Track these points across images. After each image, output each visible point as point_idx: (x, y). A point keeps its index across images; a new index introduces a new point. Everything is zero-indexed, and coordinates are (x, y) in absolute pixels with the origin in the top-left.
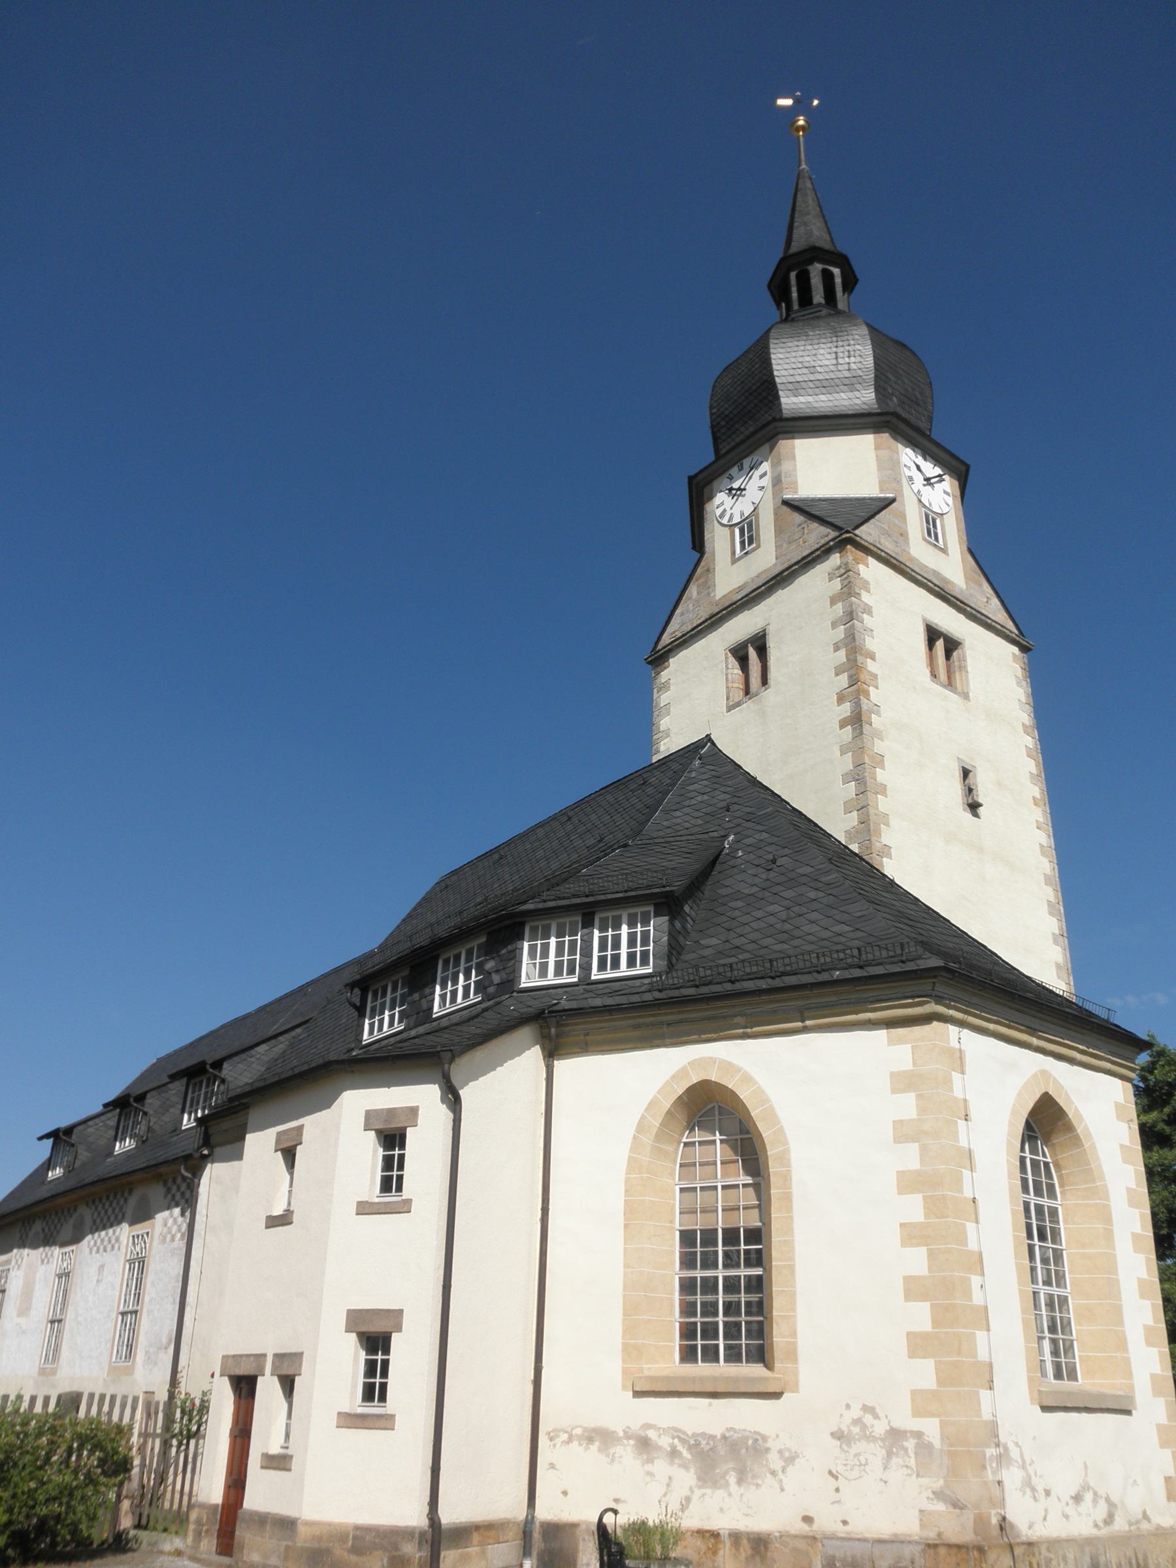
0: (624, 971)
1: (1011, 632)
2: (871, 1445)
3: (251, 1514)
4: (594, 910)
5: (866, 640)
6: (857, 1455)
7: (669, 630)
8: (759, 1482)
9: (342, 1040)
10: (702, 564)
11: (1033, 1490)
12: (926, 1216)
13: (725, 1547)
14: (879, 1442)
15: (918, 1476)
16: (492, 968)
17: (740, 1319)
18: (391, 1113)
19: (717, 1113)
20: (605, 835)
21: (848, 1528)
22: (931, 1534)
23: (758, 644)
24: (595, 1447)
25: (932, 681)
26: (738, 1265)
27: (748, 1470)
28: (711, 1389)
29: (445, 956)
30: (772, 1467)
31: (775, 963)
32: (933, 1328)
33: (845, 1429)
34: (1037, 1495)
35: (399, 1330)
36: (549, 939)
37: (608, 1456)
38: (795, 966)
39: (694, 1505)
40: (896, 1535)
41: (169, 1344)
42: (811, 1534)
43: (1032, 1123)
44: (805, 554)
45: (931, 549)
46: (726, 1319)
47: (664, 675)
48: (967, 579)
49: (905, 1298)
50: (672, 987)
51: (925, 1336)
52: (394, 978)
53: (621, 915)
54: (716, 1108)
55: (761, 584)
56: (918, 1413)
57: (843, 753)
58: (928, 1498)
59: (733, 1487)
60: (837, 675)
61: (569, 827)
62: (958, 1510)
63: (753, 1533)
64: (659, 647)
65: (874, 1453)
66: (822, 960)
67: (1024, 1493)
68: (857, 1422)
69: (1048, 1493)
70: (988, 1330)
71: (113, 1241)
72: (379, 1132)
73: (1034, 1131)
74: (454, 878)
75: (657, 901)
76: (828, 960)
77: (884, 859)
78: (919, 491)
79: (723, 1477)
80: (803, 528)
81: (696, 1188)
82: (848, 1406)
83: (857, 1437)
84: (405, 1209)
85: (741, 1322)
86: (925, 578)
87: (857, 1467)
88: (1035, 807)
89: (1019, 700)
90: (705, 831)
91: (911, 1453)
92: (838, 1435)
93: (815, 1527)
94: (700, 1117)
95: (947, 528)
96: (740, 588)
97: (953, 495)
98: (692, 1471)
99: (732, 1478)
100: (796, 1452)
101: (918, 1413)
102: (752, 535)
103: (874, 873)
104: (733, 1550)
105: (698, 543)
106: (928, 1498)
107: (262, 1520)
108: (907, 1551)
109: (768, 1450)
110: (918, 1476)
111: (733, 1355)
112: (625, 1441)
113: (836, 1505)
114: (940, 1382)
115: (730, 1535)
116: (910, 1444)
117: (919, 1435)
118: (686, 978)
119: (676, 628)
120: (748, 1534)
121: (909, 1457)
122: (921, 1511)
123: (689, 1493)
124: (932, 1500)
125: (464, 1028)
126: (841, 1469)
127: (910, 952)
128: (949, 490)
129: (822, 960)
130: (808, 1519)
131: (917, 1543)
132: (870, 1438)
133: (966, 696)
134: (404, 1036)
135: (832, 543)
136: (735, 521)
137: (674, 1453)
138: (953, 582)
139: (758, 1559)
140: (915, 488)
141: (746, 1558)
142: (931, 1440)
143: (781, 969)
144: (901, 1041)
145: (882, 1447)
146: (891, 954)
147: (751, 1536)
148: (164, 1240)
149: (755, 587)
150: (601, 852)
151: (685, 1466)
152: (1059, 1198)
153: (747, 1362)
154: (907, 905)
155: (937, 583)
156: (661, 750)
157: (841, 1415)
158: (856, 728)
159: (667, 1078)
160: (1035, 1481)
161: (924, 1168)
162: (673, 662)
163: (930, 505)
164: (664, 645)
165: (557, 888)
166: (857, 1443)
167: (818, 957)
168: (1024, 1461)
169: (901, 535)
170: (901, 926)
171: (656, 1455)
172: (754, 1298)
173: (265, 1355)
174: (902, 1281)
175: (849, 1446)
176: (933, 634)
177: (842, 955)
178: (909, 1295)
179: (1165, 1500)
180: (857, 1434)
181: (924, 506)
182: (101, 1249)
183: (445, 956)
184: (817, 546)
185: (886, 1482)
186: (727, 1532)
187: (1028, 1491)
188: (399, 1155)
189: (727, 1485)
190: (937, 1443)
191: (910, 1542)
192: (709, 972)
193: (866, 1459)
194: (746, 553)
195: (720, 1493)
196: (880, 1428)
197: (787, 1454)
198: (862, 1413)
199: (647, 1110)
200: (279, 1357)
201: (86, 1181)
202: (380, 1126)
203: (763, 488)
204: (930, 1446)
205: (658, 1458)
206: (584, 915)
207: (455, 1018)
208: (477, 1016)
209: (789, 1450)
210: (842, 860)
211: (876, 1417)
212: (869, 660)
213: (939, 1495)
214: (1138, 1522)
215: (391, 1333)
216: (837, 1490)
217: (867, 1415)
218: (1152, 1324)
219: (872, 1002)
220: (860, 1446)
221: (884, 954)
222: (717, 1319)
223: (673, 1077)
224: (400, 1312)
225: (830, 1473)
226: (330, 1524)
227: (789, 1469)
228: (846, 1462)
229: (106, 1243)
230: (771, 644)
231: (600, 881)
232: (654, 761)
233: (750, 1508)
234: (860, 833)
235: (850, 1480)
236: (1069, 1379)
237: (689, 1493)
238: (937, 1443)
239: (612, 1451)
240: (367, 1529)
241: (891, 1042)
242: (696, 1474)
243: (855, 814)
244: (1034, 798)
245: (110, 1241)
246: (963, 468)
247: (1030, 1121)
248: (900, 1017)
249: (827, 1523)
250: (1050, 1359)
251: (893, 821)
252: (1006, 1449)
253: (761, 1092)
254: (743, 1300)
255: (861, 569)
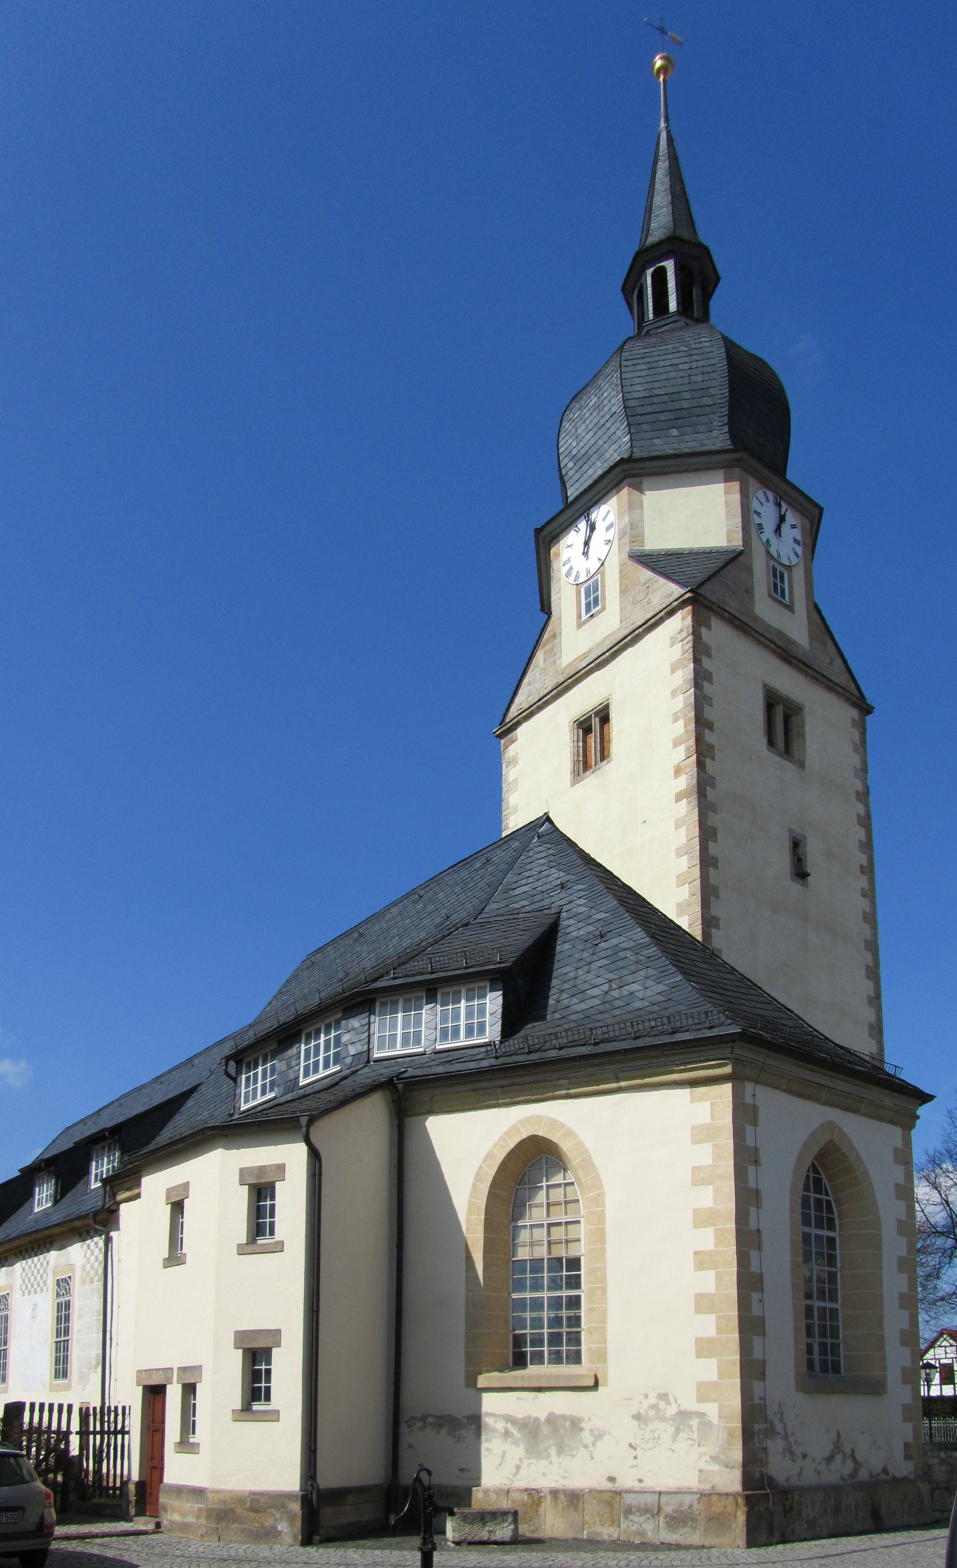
0: (463, 1041)
1: (853, 695)
2: (664, 1424)
3: (170, 1487)
4: (436, 986)
5: (705, 709)
6: (652, 1431)
7: (517, 700)
8: (574, 1453)
9: (224, 1107)
10: (549, 628)
11: (792, 1454)
12: (716, 1245)
13: (546, 1500)
14: (670, 1421)
15: (699, 1445)
16: (348, 1040)
17: (543, 1331)
18: (262, 1169)
19: (544, 1162)
20: (451, 913)
21: (642, 1485)
22: (706, 1487)
23: (602, 715)
24: (444, 1431)
25: (768, 749)
26: (561, 1288)
27: (566, 1444)
28: (536, 1385)
29: (308, 1031)
30: (585, 1441)
31: (594, 1031)
32: (717, 1334)
33: (642, 1411)
34: (795, 1457)
35: (279, 1345)
36: (422, 1010)
37: (454, 1437)
38: (612, 1034)
39: (523, 1471)
40: (679, 1488)
41: (98, 1365)
42: (613, 1489)
43: (817, 1165)
44: (649, 616)
45: (777, 606)
46: (550, 1331)
47: (512, 751)
48: (812, 637)
49: (695, 1311)
50: (505, 1054)
51: (711, 1341)
52: (264, 1052)
53: (398, 1000)
54: (544, 1158)
55: (605, 650)
56: (701, 1399)
57: (677, 827)
58: (706, 1461)
59: (554, 1458)
60: (675, 746)
61: (420, 906)
62: (729, 1470)
63: (569, 1490)
64: (508, 720)
65: (665, 1430)
66: (636, 1028)
67: (784, 1457)
68: (654, 1407)
69: (804, 1456)
70: (764, 1335)
71: (42, 1285)
72: (252, 1186)
73: (819, 1173)
74: (319, 956)
75: (492, 977)
76: (641, 1027)
77: (713, 930)
78: (768, 541)
79: (546, 1450)
80: (648, 587)
81: (527, 1225)
82: (646, 1396)
83: (652, 1418)
84: (278, 1249)
85: (563, 1332)
86: (768, 639)
87: (651, 1441)
88: (860, 874)
89: (855, 767)
90: (540, 909)
91: (695, 1429)
92: (637, 1417)
93: (617, 1485)
94: (530, 1167)
95: (795, 585)
96: (585, 655)
97: (804, 544)
98: (522, 1446)
99: (553, 1451)
100: (603, 1430)
101: (701, 1399)
102: (598, 596)
103: (696, 945)
104: (553, 1503)
105: (546, 607)
106: (706, 1461)
107: (179, 1490)
108: (687, 1499)
109: (581, 1429)
110: (699, 1445)
111: (557, 1358)
112: (469, 1426)
113: (634, 1468)
114: (721, 1376)
115: (550, 1492)
116: (694, 1422)
117: (701, 1415)
118: (517, 1046)
119: (522, 700)
120: (564, 1491)
121: (693, 1432)
122: (701, 1471)
123: (519, 1463)
124: (709, 1463)
125: (322, 1095)
126: (639, 1442)
127: (713, 1020)
128: (799, 538)
129: (636, 1028)
130: (612, 1479)
131: (696, 1493)
132: (662, 1419)
133: (801, 765)
134: (275, 1102)
135: (676, 603)
136: (581, 580)
137: (507, 1434)
138: (797, 643)
139: (572, 1508)
140: (764, 537)
141: (563, 1508)
142: (711, 1419)
143: (600, 1037)
144: (702, 1099)
145: (672, 1425)
146: (696, 1021)
147: (567, 1492)
148: (84, 1283)
149: (600, 653)
150: (447, 930)
151: (516, 1443)
152: (837, 1230)
153: (567, 1363)
154: (722, 975)
155: (780, 644)
156: (510, 826)
157: (641, 1403)
158: (691, 800)
159: (501, 1133)
160: (794, 1447)
161: (716, 1206)
162: (521, 731)
163: (779, 556)
164: (513, 717)
165: (404, 967)
166: (653, 1422)
167: (632, 1026)
168: (786, 1433)
169: (747, 591)
170: (713, 995)
171: (493, 1436)
172: (571, 1313)
173: (172, 1369)
174: (693, 1297)
175: (646, 1425)
176: (772, 700)
177: (653, 1024)
178: (698, 1309)
179: (902, 1458)
180: (652, 1416)
181: (772, 557)
182: (32, 1292)
183: (308, 1031)
184: (661, 608)
185: (674, 1451)
186: (548, 1490)
187: (788, 1455)
188: (270, 1204)
189: (549, 1456)
190: (715, 1420)
191: (691, 1493)
192: (536, 1041)
193: (659, 1434)
194: (592, 616)
195: (543, 1462)
196: (671, 1410)
197: (597, 1433)
198: (657, 1400)
199: (484, 1161)
200: (183, 1370)
201: (12, 1236)
202: (252, 1181)
203: (610, 541)
204: (709, 1424)
205: (494, 1437)
206: (428, 991)
207: (318, 1087)
208: (336, 1084)
209: (598, 1429)
210: (664, 934)
211: (669, 1403)
212: (707, 731)
213: (714, 1459)
214: (877, 1475)
215: (271, 1348)
216: (635, 1458)
217: (661, 1402)
218: (908, 1329)
219: (678, 1065)
220: (656, 1425)
221: (690, 1021)
222: (543, 1331)
223: (506, 1133)
224: (279, 1331)
225: (630, 1445)
226: (232, 1492)
227: (599, 1444)
228: (642, 1437)
229: (35, 1286)
230: (613, 715)
231: (455, 956)
232: (503, 836)
233: (566, 1472)
234: (691, 905)
235: (645, 1450)
236: (833, 1372)
237: (519, 1463)
238: (715, 1420)
239: (458, 1433)
240: (261, 1494)
241: (693, 1100)
242: (524, 1448)
243: (687, 886)
244: (861, 866)
245: (39, 1285)
246: (817, 512)
247: (815, 1162)
248: (702, 1078)
249: (626, 1481)
250: (818, 1357)
251: (723, 894)
252: (772, 1424)
253: (580, 1144)
254: (545, 1313)
255: (703, 633)
